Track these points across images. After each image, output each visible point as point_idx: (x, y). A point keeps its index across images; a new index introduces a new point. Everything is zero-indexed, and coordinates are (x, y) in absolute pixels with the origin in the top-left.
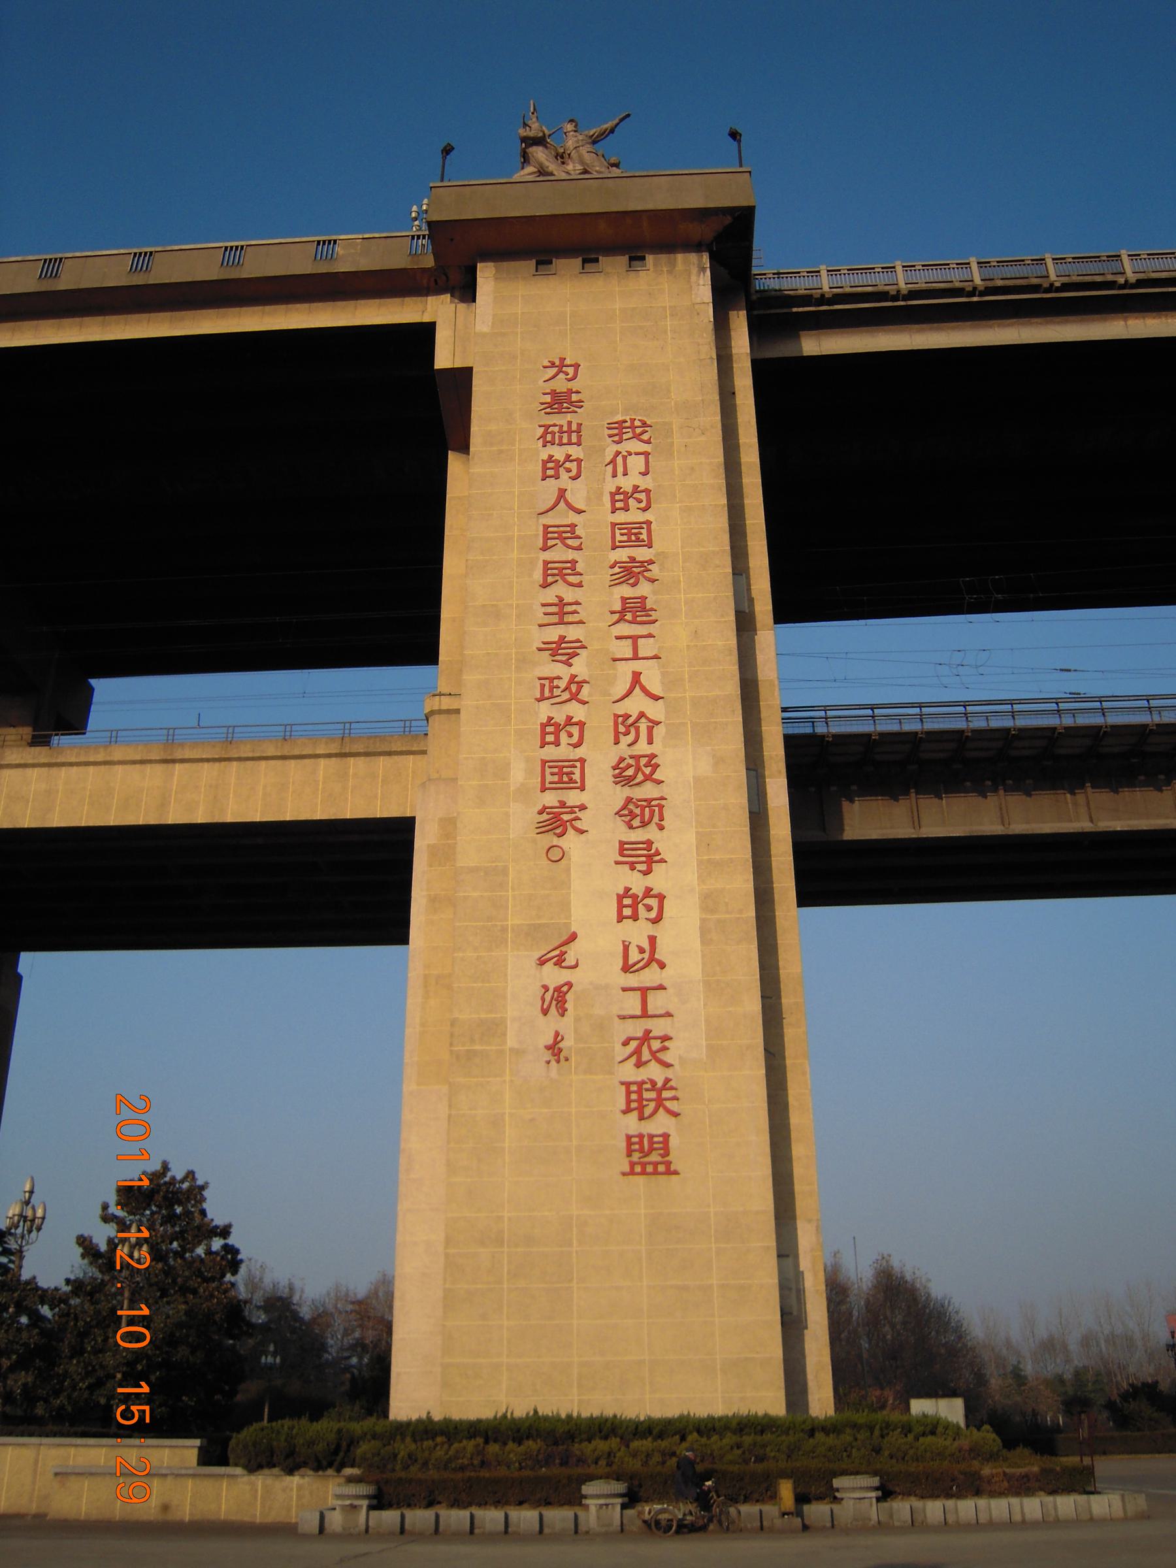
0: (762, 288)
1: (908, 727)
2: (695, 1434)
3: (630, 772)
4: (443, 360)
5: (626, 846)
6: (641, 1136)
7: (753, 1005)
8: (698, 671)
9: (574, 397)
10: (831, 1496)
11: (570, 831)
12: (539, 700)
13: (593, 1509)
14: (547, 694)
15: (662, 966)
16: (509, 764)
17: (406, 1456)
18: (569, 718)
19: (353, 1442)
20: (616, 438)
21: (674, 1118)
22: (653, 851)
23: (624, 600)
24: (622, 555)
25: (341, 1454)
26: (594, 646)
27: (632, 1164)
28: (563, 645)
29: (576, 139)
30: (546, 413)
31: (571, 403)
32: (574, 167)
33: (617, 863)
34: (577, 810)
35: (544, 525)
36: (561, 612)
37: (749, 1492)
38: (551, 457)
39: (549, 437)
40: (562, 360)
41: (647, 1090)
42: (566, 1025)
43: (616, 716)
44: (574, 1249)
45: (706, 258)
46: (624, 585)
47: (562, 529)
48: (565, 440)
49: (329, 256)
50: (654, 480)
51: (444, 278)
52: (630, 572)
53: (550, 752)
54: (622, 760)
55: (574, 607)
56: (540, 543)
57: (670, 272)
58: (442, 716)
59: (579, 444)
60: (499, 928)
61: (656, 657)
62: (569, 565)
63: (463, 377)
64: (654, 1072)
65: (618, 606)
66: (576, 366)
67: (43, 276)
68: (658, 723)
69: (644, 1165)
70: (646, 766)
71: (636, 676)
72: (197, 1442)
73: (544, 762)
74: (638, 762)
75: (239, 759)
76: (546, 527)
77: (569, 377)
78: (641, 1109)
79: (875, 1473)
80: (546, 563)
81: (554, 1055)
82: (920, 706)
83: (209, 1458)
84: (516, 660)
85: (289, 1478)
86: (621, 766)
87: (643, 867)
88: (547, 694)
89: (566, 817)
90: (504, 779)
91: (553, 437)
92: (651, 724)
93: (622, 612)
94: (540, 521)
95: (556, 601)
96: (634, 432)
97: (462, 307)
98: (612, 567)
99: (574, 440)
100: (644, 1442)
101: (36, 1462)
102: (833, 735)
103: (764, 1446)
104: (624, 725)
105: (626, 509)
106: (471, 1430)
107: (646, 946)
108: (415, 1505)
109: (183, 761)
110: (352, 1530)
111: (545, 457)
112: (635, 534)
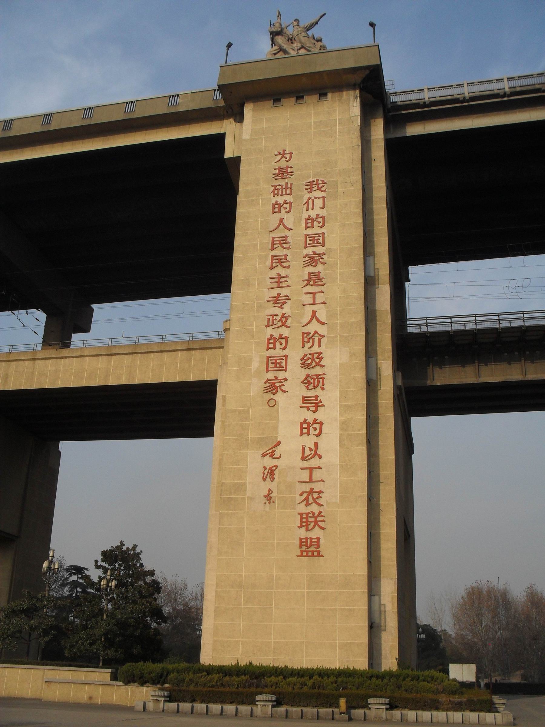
0: (394, 101)
1: (469, 327)
2: (317, 676)
3: (309, 361)
4: (228, 153)
5: (305, 398)
6: (307, 539)
7: (363, 476)
8: (344, 309)
9: (289, 170)
10: (366, 706)
11: (280, 391)
12: (267, 327)
13: (259, 707)
14: (271, 323)
15: (320, 457)
16: (252, 359)
17: (189, 680)
18: (281, 335)
19: (168, 673)
20: (309, 190)
21: (322, 530)
22: (318, 401)
23: (310, 274)
24: (309, 251)
25: (163, 678)
26: (294, 298)
28: (279, 298)
29: (297, 30)
30: (275, 179)
31: (288, 173)
32: (297, 45)
33: (301, 407)
34: (283, 381)
35: (272, 237)
36: (279, 281)
37: (332, 703)
38: (277, 202)
39: (276, 192)
40: (284, 151)
41: (310, 517)
42: (274, 486)
43: (304, 333)
44: (274, 590)
45: (358, 92)
47: (281, 239)
48: (284, 193)
49: (175, 104)
50: (327, 211)
51: (231, 110)
52: (313, 260)
53: (271, 353)
54: (305, 355)
55: (285, 279)
56: (270, 247)
57: (339, 100)
59: (291, 194)
60: (245, 439)
61: (324, 303)
62: (284, 257)
63: (237, 161)
64: (314, 508)
65: (306, 278)
66: (291, 154)
67: (44, 123)
68: (323, 336)
69: (307, 552)
70: (317, 358)
71: (314, 313)
72: (110, 670)
73: (268, 357)
74: (313, 357)
75: (141, 353)
76: (273, 238)
77: (287, 159)
79: (386, 697)
80: (273, 256)
81: (267, 500)
82: (475, 316)
83: (114, 677)
84: (257, 306)
85: (142, 688)
86: (305, 358)
87: (313, 409)
88: (271, 323)
89: (277, 385)
90: (249, 366)
91: (278, 192)
92: (320, 337)
93: (308, 280)
94: (270, 235)
95: (276, 276)
96: (318, 187)
97: (238, 125)
98: (304, 257)
99: (288, 192)
100: (293, 679)
101: (43, 676)
102: (430, 333)
103: (347, 683)
104: (307, 338)
105: (312, 227)
106: (219, 670)
107: (313, 447)
108: (186, 701)
109: (115, 354)
110: (157, 710)
111: (274, 202)
112: (316, 240)
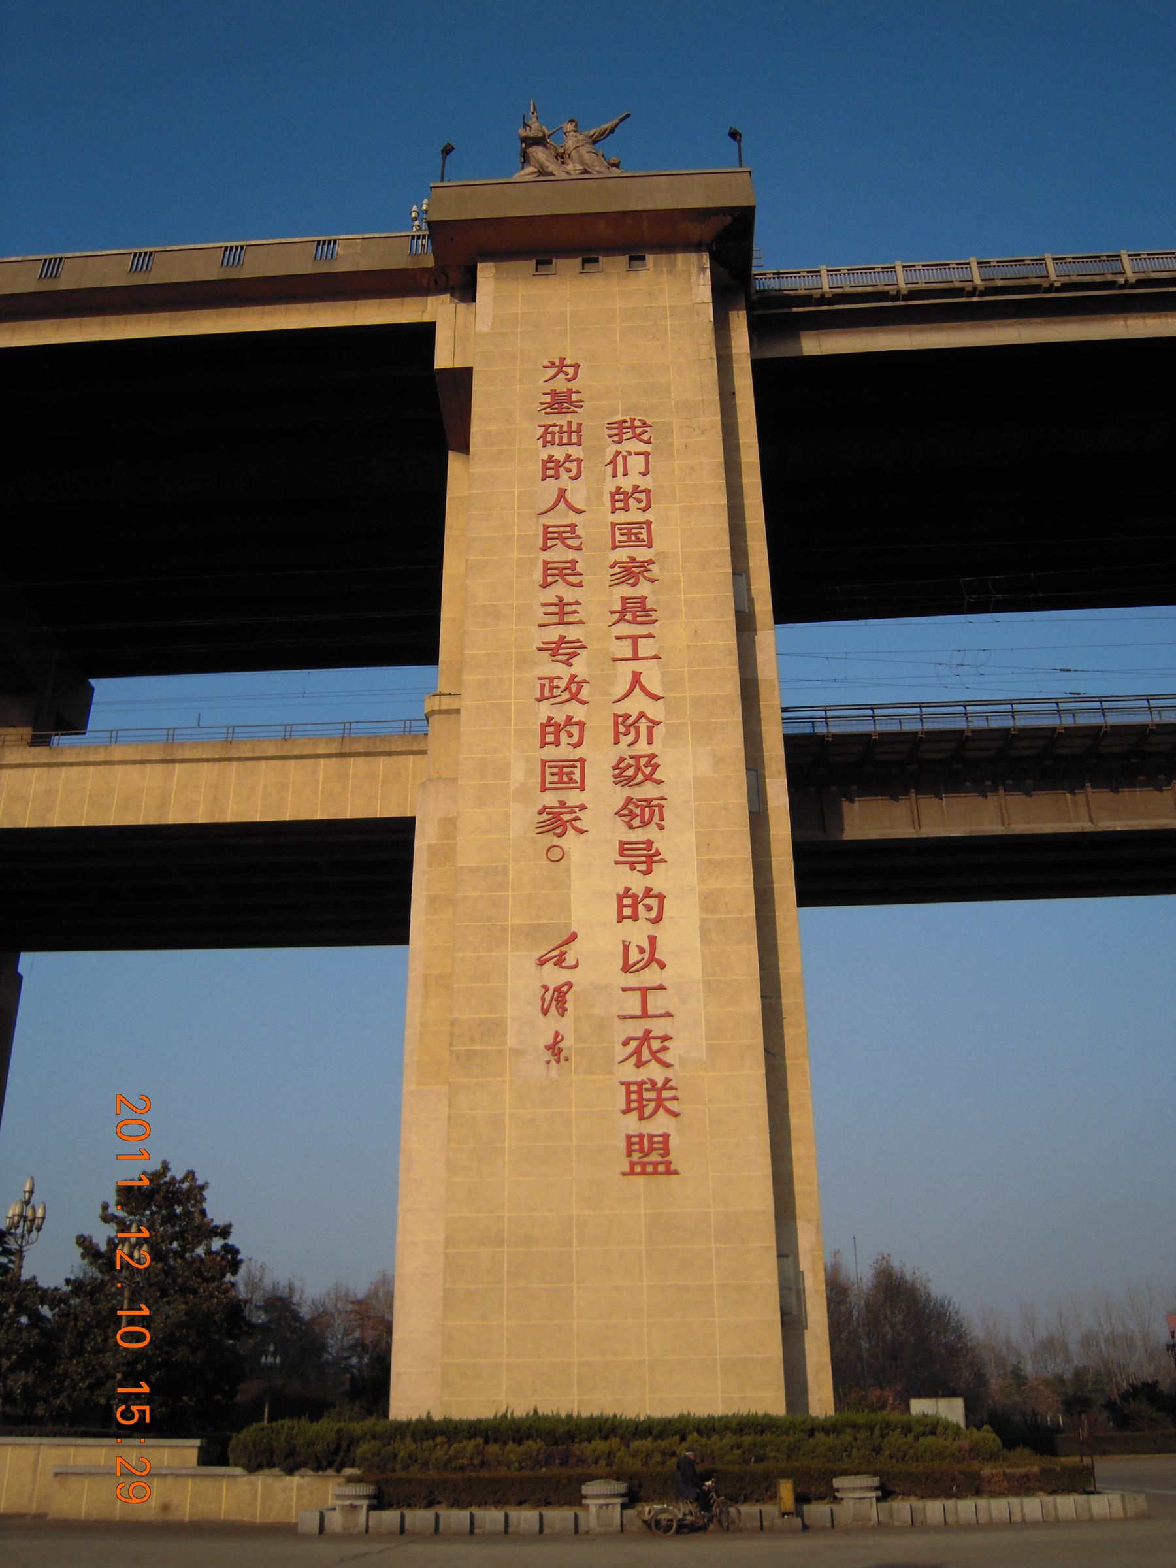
0: (762, 288)
1: (908, 727)
2: (695, 1434)
3: (630, 772)
4: (443, 360)
5: (626, 846)
6: (641, 1136)
7: (753, 1005)
8: (698, 671)
9: (574, 397)
10: (831, 1496)
11: (570, 831)
12: (539, 700)
13: (593, 1509)
14: (547, 694)
15: (662, 966)
16: (509, 764)
17: (406, 1456)
18: (569, 718)
19: (353, 1442)
20: (616, 438)
21: (674, 1118)
22: (653, 851)
23: (624, 600)
24: (622, 555)
25: (341, 1454)
26: (594, 646)
27: (632, 1164)
28: (563, 645)
29: (576, 139)
30: (546, 413)
31: (571, 403)
32: (574, 167)
33: (617, 863)
34: (577, 810)
35: (544, 525)
36: (561, 612)
37: (749, 1492)
38: (551, 457)
39: (549, 437)
40: (562, 360)
41: (647, 1090)
42: (566, 1025)
43: (616, 716)
44: (574, 1249)
45: (706, 258)
46: (624, 585)
47: (562, 529)
48: (565, 440)
49: (329, 256)
50: (654, 480)
51: (444, 278)
52: (630, 572)
53: (550, 752)
54: (622, 760)
55: (574, 607)
56: (540, 543)
57: (670, 272)
58: (442, 716)
59: (579, 444)
60: (499, 928)
61: (656, 657)
62: (569, 565)
63: (463, 377)
64: (654, 1072)
65: (618, 606)
66: (576, 366)
67: (43, 276)
68: (658, 723)
69: (644, 1165)
70: (646, 766)
71: (636, 676)
72: (197, 1442)
73: (544, 762)
74: (638, 762)
75: (239, 759)
76: (546, 527)
77: (569, 377)
78: (641, 1109)
79: (875, 1473)
80: (546, 563)
81: (554, 1055)
82: (920, 706)
83: (209, 1458)
84: (516, 660)
85: (289, 1478)
86: (621, 766)
87: (643, 867)
88: (547, 694)
89: (566, 817)
90: (504, 779)
91: (553, 437)
92: (651, 724)
93: (622, 612)
94: (540, 521)
95: (556, 601)
96: (634, 432)
97: (462, 307)
98: (612, 567)
99: (574, 440)
100: (644, 1442)
101: (36, 1462)
102: (833, 735)
103: (764, 1446)
104: (624, 725)
105: (626, 509)
106: (471, 1430)
107: (646, 946)
108: (415, 1505)
109: (183, 761)
110: (352, 1530)
111: (545, 457)
112: (635, 534)
